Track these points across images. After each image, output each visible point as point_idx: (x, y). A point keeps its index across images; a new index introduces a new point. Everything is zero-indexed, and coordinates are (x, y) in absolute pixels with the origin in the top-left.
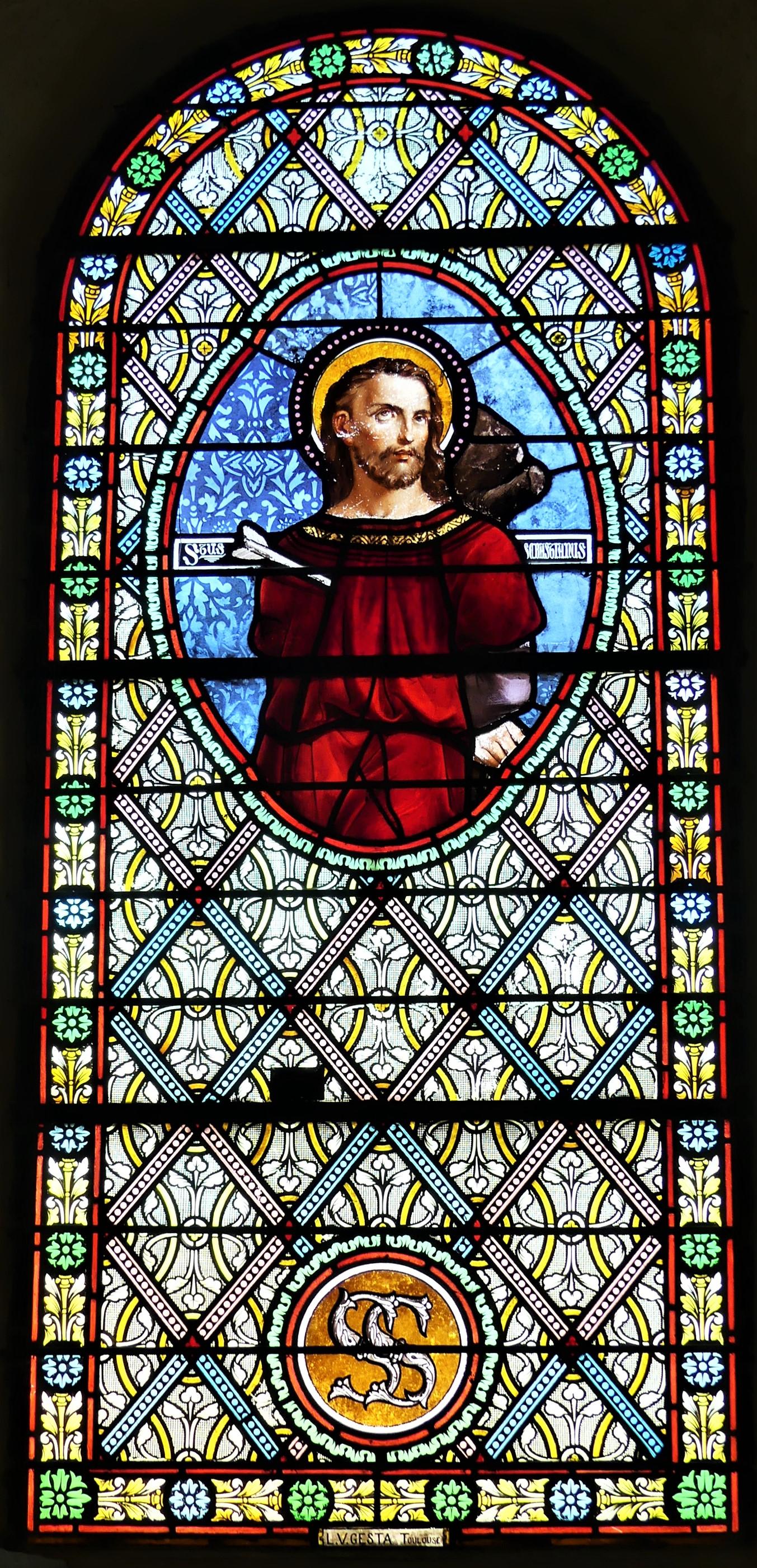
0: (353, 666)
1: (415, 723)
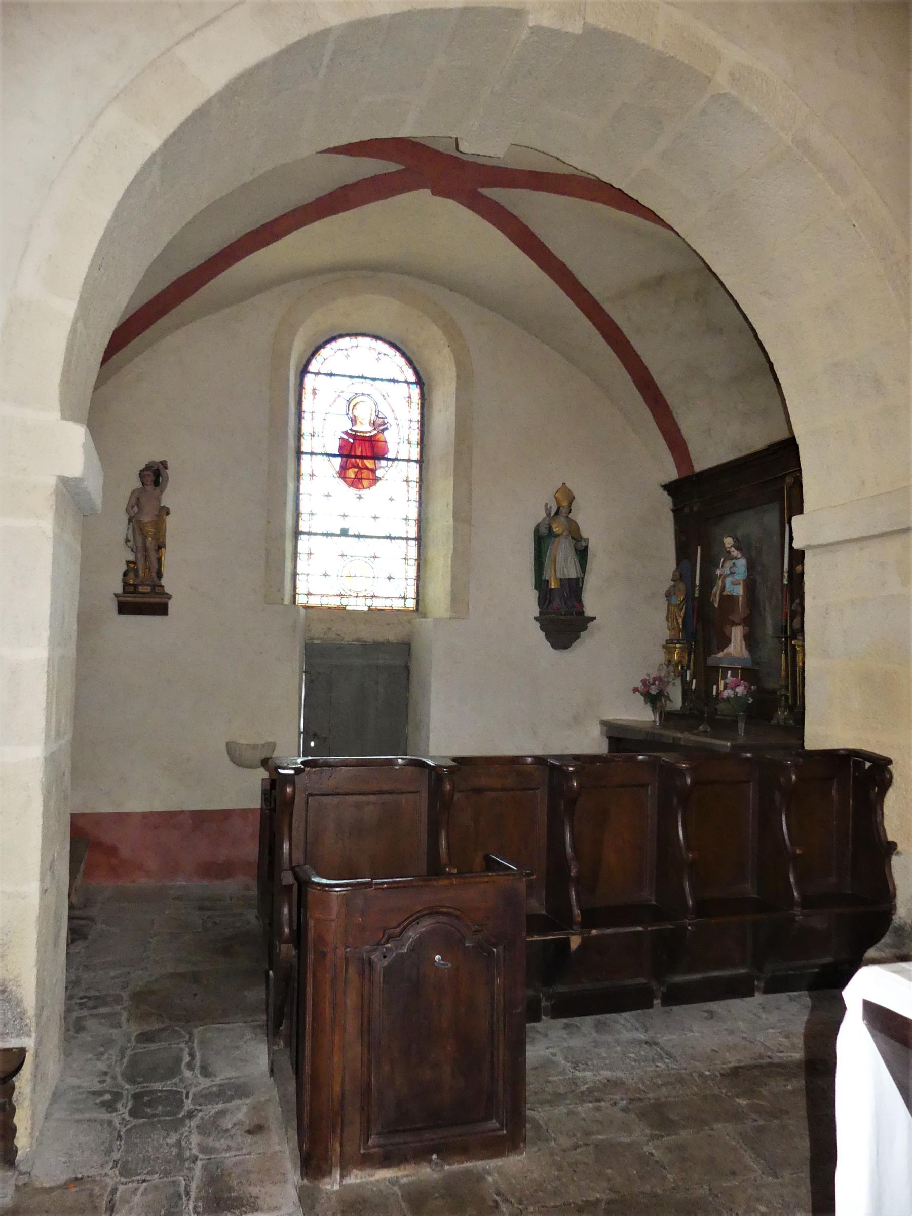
0: (356, 457)
1: (367, 468)
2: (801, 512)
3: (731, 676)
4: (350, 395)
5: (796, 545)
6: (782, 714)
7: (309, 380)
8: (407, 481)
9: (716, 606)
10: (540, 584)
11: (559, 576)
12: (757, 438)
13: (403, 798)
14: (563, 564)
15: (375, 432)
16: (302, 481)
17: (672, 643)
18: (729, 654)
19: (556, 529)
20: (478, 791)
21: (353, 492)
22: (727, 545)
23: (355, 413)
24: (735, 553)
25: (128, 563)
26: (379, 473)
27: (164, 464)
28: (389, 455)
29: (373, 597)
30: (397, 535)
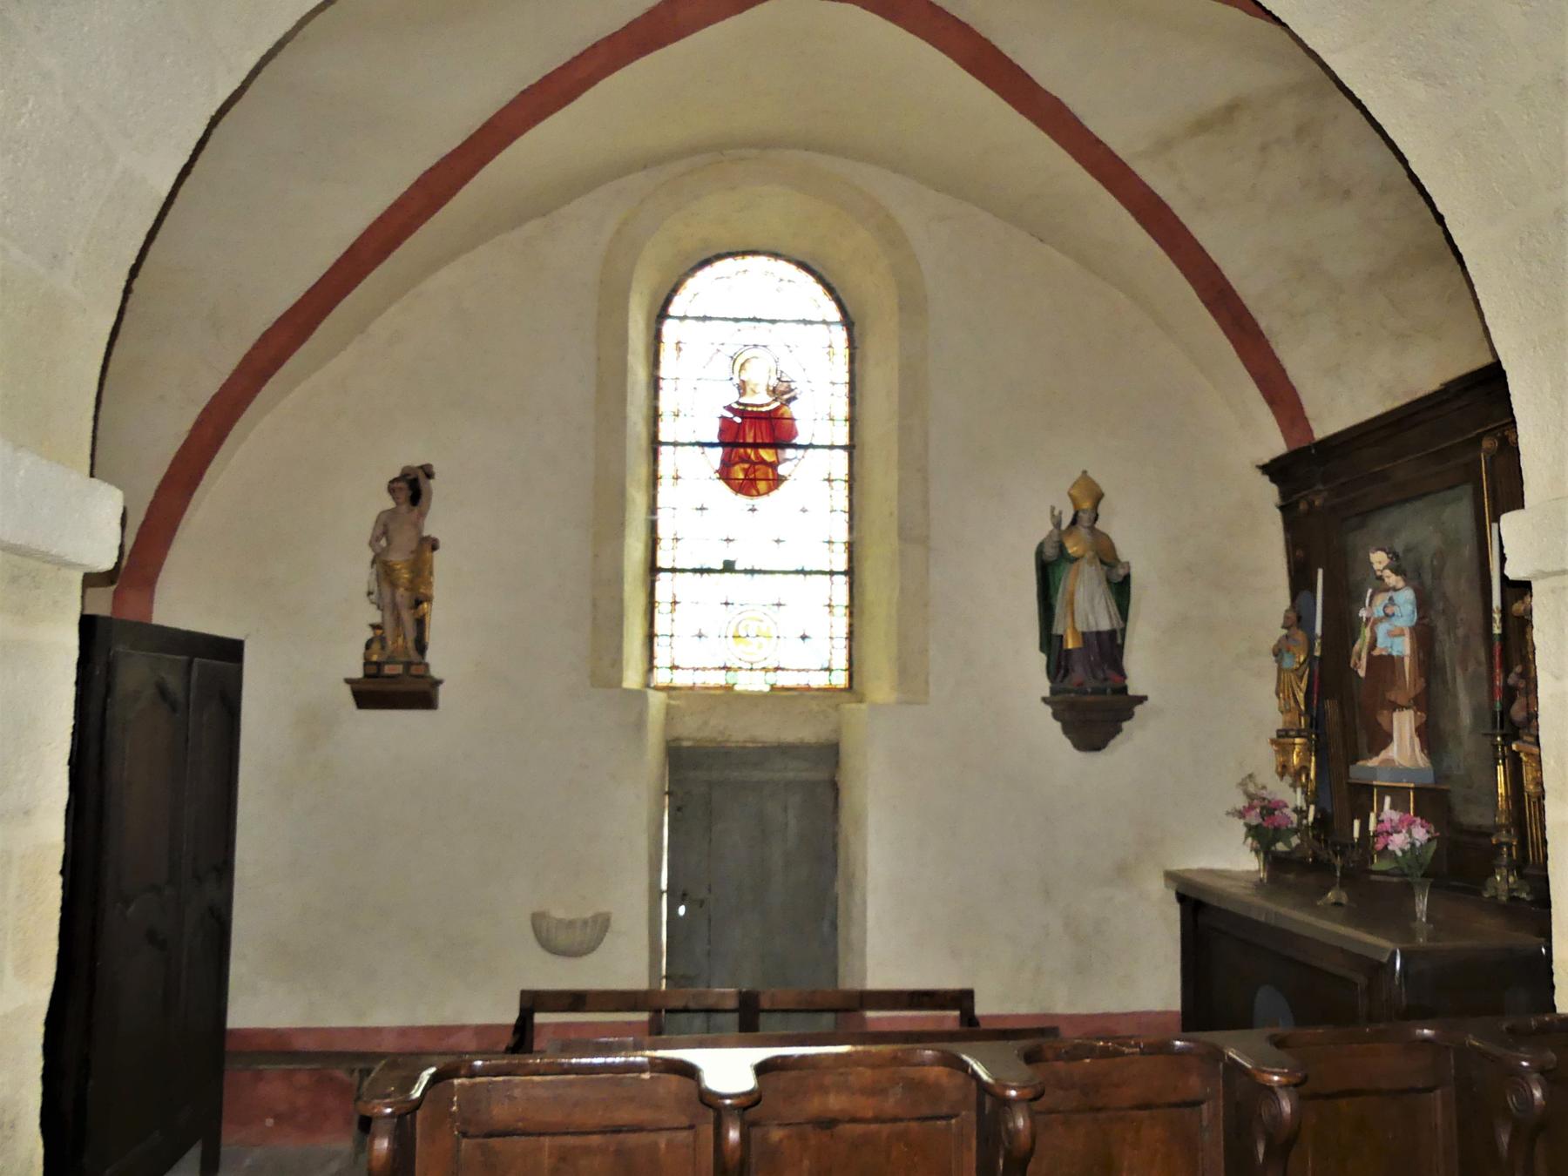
0: (745, 445)
1: (763, 462)
2: (1517, 502)
3: (1393, 807)
4: (736, 349)
5: (1513, 573)
6: (1502, 881)
7: (670, 329)
8: (829, 480)
9: (1362, 673)
10: (1049, 641)
11: (1081, 627)
12: (1424, 371)
13: (662, 1140)
14: (1087, 609)
15: (777, 404)
16: (660, 489)
17: (1287, 736)
18: (1390, 761)
19: (1072, 549)
20: (827, 1123)
21: (743, 501)
22: (1377, 566)
23: (744, 377)
24: (1392, 579)
25: (374, 627)
26: (782, 470)
27: (428, 472)
28: (797, 441)
29: (777, 669)
30: (815, 569)
